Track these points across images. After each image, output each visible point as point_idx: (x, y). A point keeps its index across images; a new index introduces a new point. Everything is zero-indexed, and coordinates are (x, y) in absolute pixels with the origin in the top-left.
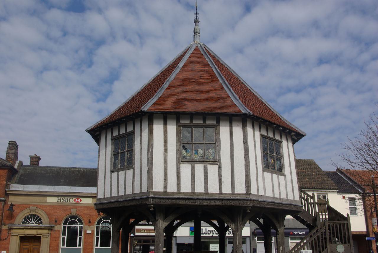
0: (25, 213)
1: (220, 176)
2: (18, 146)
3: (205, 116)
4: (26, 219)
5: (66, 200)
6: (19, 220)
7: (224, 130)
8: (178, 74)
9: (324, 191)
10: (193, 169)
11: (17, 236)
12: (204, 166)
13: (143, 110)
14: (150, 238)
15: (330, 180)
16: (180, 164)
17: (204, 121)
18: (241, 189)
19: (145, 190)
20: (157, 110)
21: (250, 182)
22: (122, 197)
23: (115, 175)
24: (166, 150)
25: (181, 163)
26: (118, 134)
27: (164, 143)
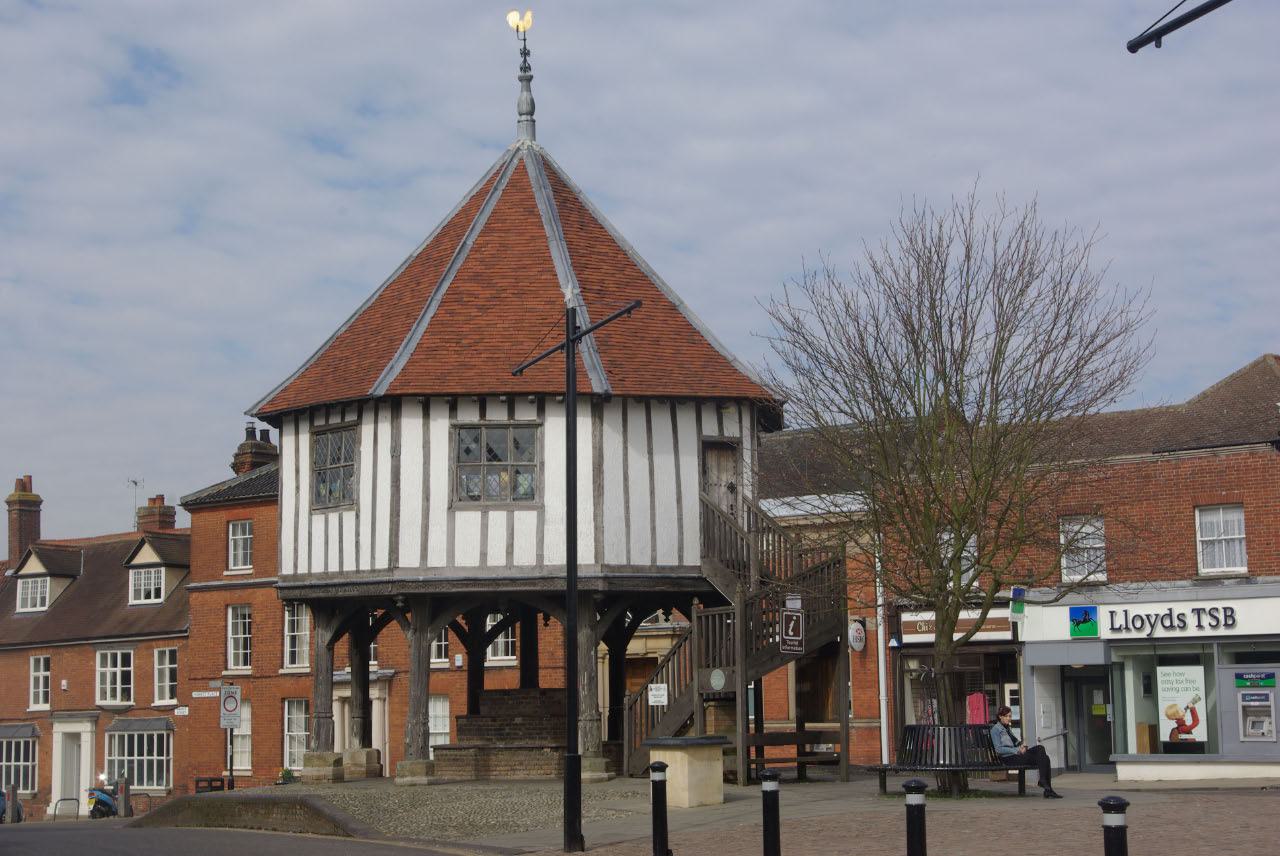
7: (131, 571)
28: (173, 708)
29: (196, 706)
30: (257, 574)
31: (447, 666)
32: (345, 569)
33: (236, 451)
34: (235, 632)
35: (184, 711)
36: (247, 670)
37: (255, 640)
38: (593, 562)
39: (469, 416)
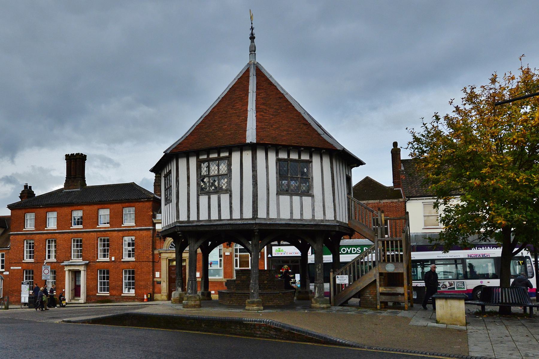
1: (231, 203)
3: (218, 150)
9: (429, 199)
10: (209, 199)
24: (189, 185)
28: (3, 272)
29: (12, 272)
30: (137, 226)
31: (109, 260)
32: (191, 219)
33: (21, 192)
34: (27, 248)
35: (8, 273)
36: (107, 294)
37: (35, 251)
38: (333, 219)
39: (283, 156)
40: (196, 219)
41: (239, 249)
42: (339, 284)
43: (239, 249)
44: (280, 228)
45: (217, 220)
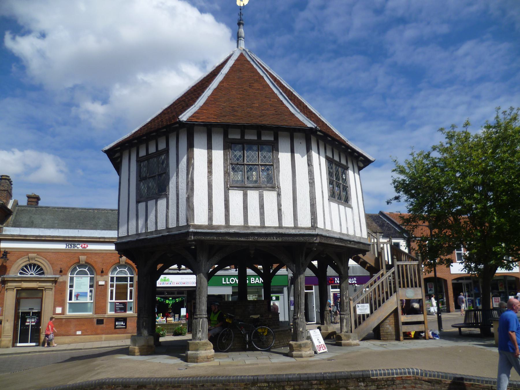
0: (22, 262)
1: (279, 205)
2: (12, 181)
4: (23, 270)
5: (74, 246)
6: (14, 272)
8: (222, 82)
10: (245, 196)
11: (13, 289)
12: (260, 192)
13: (181, 120)
14: (175, 289)
15: (374, 223)
16: (229, 189)
17: (259, 136)
18: (305, 222)
19: (183, 222)
20: (200, 121)
21: (316, 214)
22: (151, 233)
23: (142, 205)
24: (210, 172)
25: (231, 188)
26: (145, 154)
27: (208, 163)
40: (242, 223)
41: (116, 277)
42: (360, 315)
43: (116, 277)
44: (336, 243)
45: (259, 227)
